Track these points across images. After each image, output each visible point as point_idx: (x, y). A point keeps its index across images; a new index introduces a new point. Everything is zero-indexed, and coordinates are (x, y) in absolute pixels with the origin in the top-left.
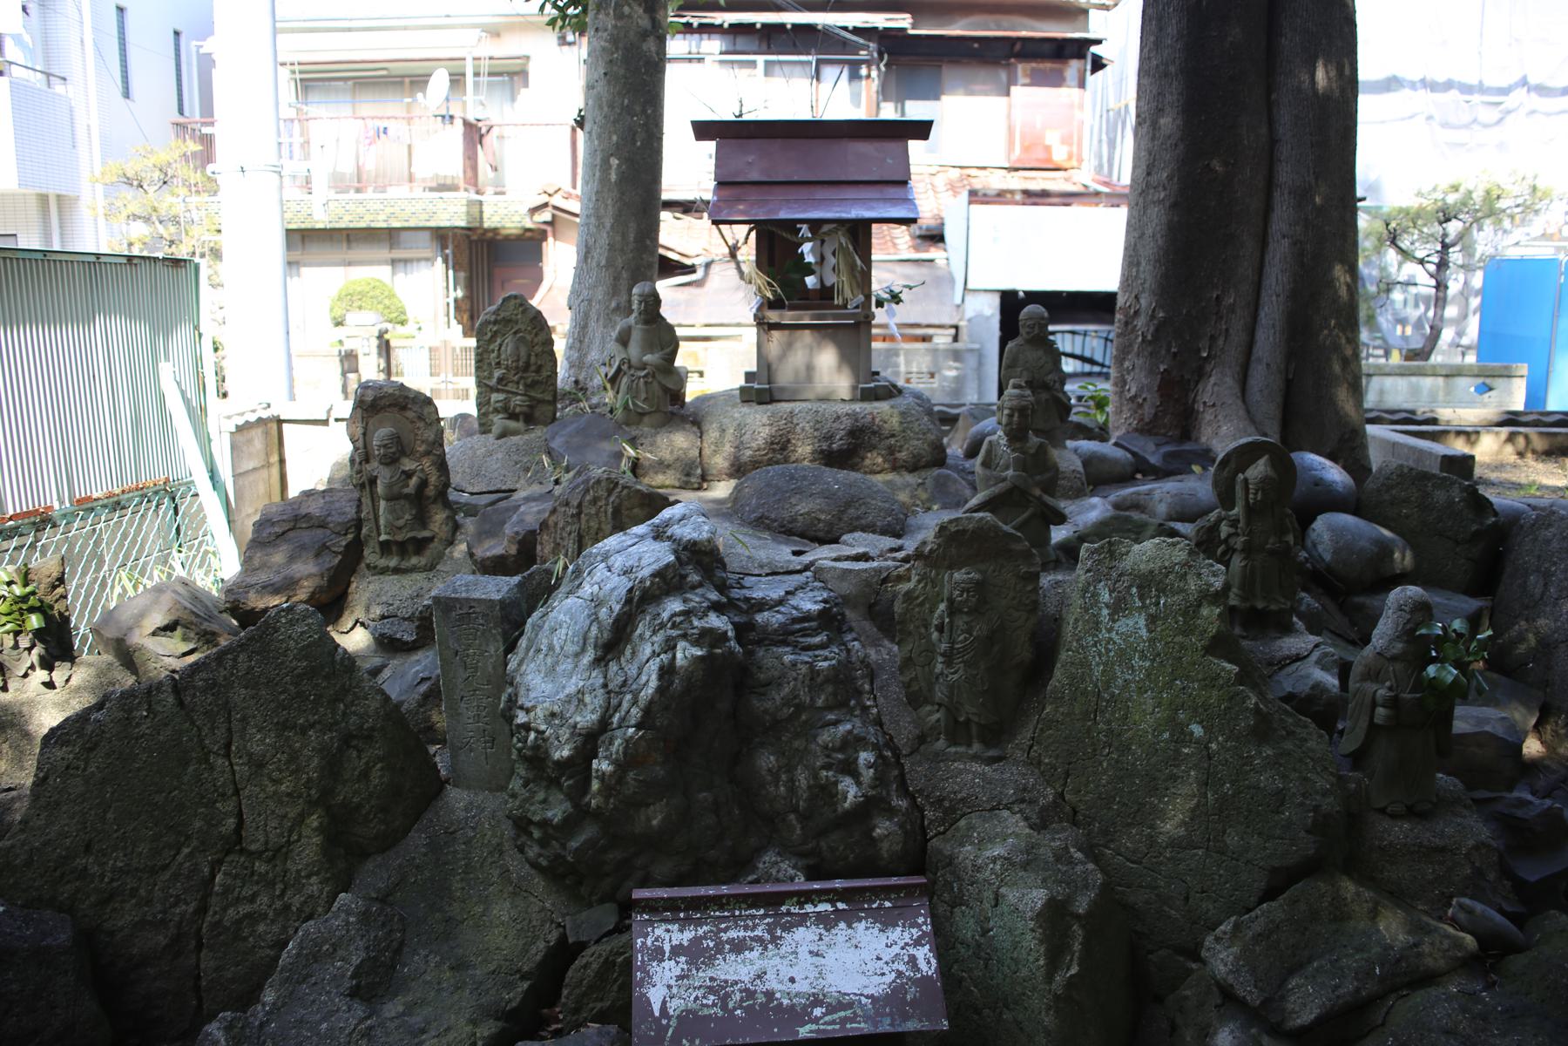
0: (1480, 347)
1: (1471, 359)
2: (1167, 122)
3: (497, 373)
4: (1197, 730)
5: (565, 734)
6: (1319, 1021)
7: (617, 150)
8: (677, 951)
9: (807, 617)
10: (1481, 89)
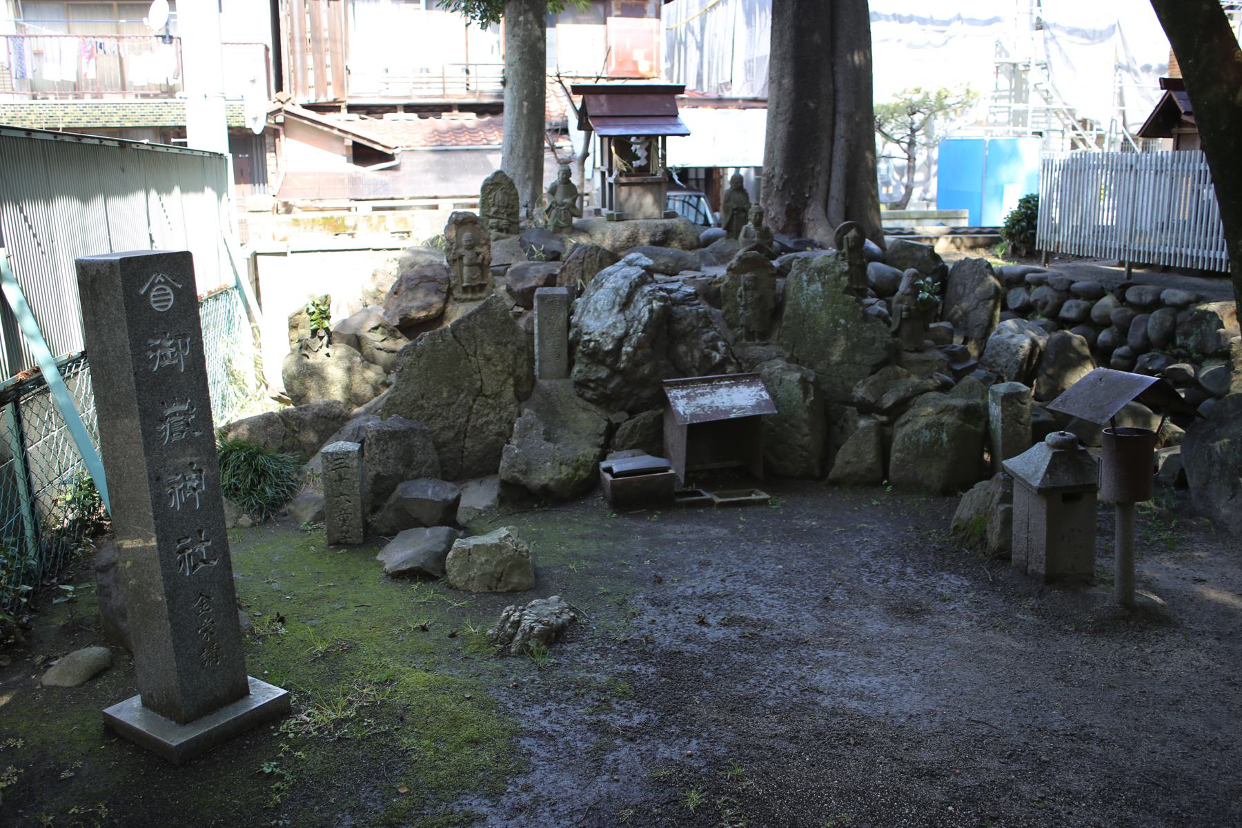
0: (939, 200)
1: (933, 208)
2: (787, 82)
3: (493, 209)
4: (842, 321)
5: (609, 340)
6: (894, 404)
7: (527, 98)
8: (682, 397)
9: (690, 294)
10: (932, 21)
